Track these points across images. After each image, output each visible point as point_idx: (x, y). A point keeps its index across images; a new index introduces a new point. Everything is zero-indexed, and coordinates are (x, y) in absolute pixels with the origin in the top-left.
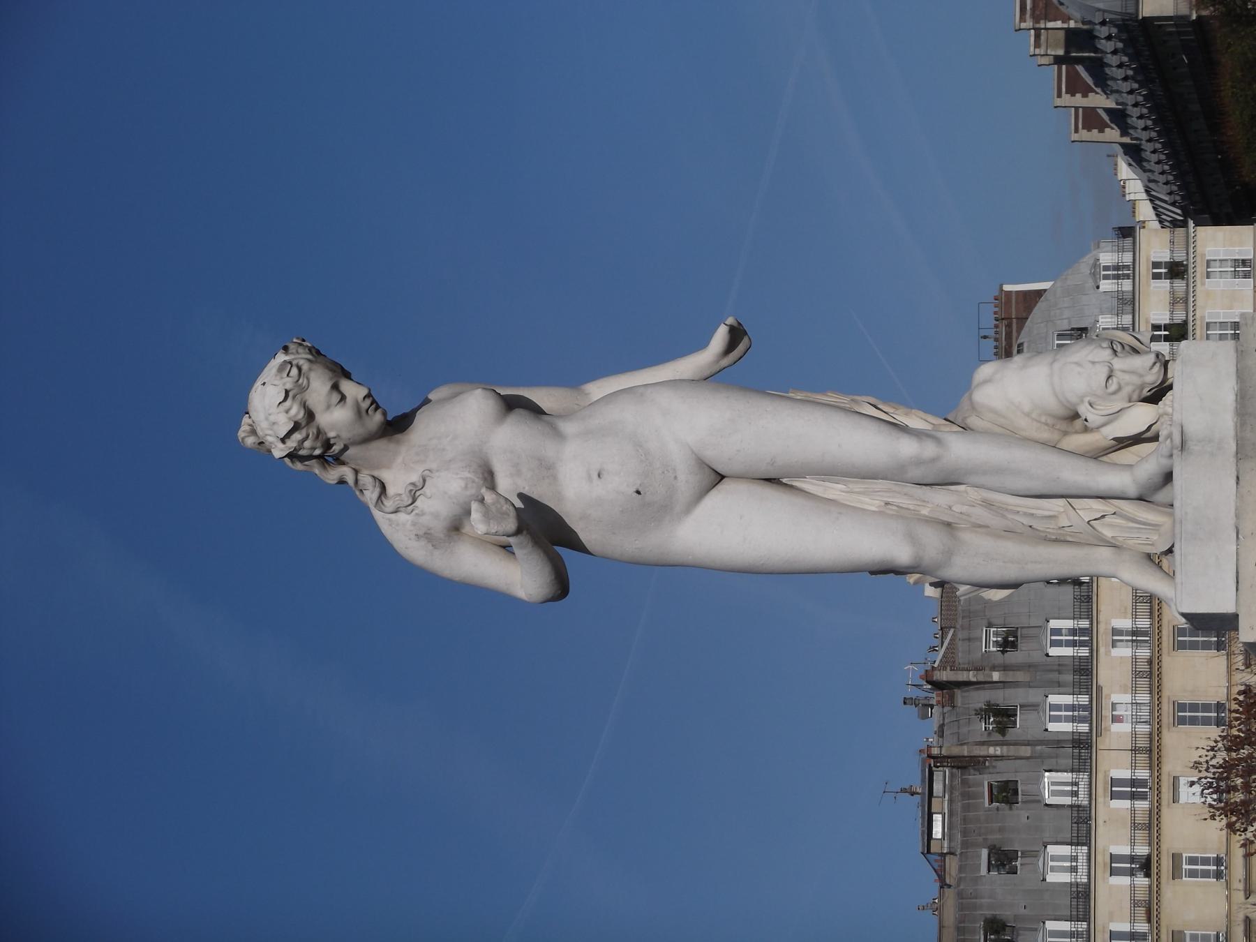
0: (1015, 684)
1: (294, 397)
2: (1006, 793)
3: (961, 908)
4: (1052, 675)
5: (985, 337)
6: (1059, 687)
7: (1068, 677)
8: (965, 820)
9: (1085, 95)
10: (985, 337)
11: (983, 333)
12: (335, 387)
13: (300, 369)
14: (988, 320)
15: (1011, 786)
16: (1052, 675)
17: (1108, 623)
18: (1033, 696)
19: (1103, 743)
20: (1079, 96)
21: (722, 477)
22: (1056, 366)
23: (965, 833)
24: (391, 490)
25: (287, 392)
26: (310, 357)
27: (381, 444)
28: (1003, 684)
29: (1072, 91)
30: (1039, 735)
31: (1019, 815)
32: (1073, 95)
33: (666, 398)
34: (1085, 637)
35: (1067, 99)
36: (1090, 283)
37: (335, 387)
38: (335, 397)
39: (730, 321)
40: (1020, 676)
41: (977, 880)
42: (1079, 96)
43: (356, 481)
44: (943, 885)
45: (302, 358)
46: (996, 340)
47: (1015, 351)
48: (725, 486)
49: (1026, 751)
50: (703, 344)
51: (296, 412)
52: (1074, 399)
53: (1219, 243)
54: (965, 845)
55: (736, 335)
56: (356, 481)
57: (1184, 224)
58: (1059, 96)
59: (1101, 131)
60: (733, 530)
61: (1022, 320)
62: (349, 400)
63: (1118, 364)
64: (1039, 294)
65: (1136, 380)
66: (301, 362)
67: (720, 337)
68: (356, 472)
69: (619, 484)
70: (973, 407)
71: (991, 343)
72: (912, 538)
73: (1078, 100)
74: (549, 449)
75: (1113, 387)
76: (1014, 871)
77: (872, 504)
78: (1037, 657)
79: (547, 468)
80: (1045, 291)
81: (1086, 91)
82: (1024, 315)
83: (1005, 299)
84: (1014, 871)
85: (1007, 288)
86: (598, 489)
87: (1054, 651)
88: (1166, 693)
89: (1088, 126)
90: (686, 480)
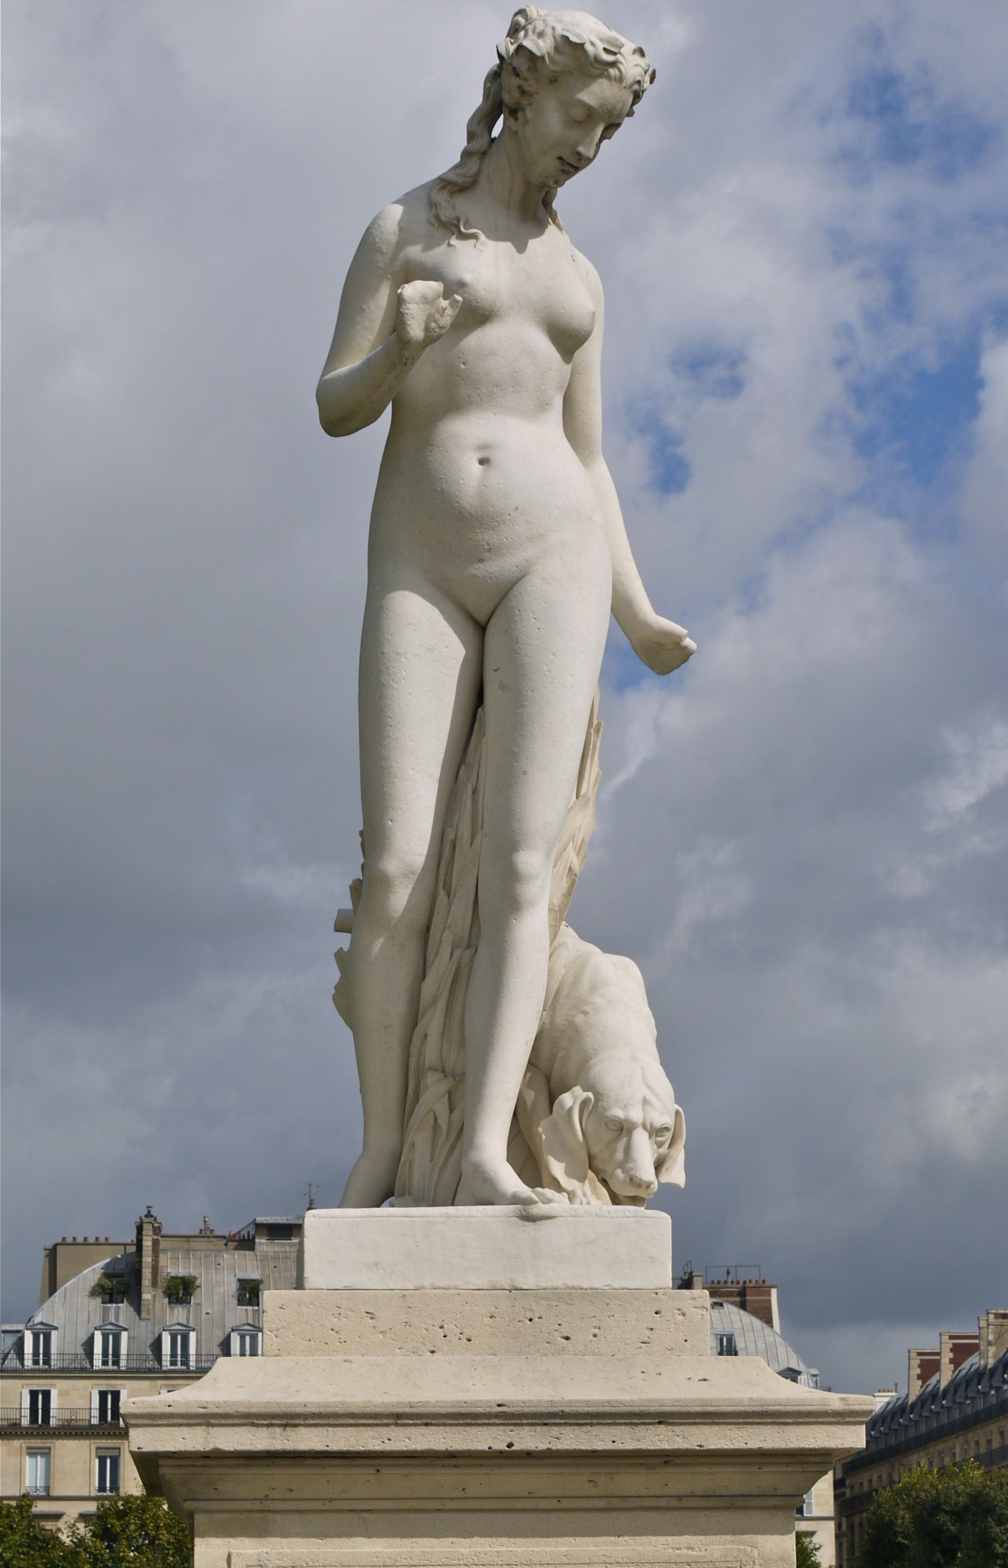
5: (728, 1273)
9: (951, 1361)
10: (728, 1273)
11: (732, 1270)
14: (745, 1275)
15: (254, 1299)
17: (54, 1385)
20: (951, 1355)
24: (460, 200)
29: (955, 1349)
32: (952, 1350)
35: (948, 1344)
42: (951, 1355)
46: (726, 1282)
47: (715, 1300)
58: (951, 1337)
59: (919, 1377)
61: (743, 1306)
64: (769, 1321)
71: (723, 1277)
73: (947, 1356)
76: (93, 1293)
80: (772, 1326)
81: (956, 1362)
82: (748, 1308)
83: (763, 1289)
84: (93, 1293)
85: (774, 1292)
89: (922, 1365)
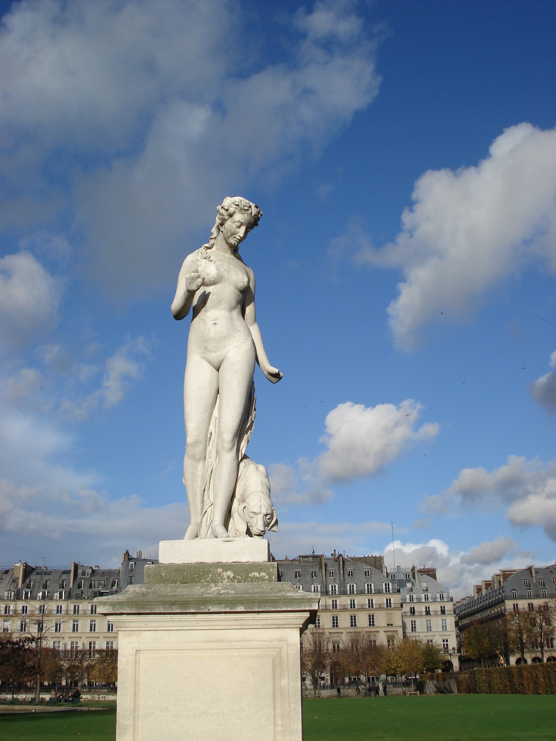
0: (340, 577)
1: (236, 208)
2: (314, 574)
3: (286, 565)
4: (343, 585)
6: (340, 587)
7: (342, 589)
8: (307, 566)
12: (242, 224)
13: (247, 210)
16: (343, 585)
18: (338, 581)
19: (327, 598)
21: (218, 370)
22: (260, 493)
23: (304, 566)
24: (209, 251)
25: (238, 205)
26: (253, 214)
27: (226, 246)
28: (340, 574)
29: (486, 585)
30: (328, 583)
31: (309, 578)
33: (246, 346)
34: (352, 593)
36: (438, 591)
37: (242, 224)
38: (238, 224)
39: (281, 374)
40: (342, 578)
41: (293, 569)
43: (212, 239)
44: (293, 560)
45: (254, 211)
48: (215, 371)
49: (324, 580)
50: (272, 364)
51: (232, 210)
52: (247, 501)
53: (451, 621)
54: (301, 565)
55: (277, 376)
56: (212, 239)
57: (455, 613)
60: (197, 376)
62: (238, 230)
63: (260, 517)
65: (254, 524)
66: (250, 211)
67: (275, 370)
68: (215, 238)
69: (213, 331)
70: (248, 465)
72: (195, 444)
73: (484, 586)
74: (225, 306)
75: (252, 515)
77: (212, 428)
78: (347, 581)
79: (216, 306)
81: (486, 588)
86: (210, 323)
87: (348, 585)
88: (340, 613)
90: (215, 356)
